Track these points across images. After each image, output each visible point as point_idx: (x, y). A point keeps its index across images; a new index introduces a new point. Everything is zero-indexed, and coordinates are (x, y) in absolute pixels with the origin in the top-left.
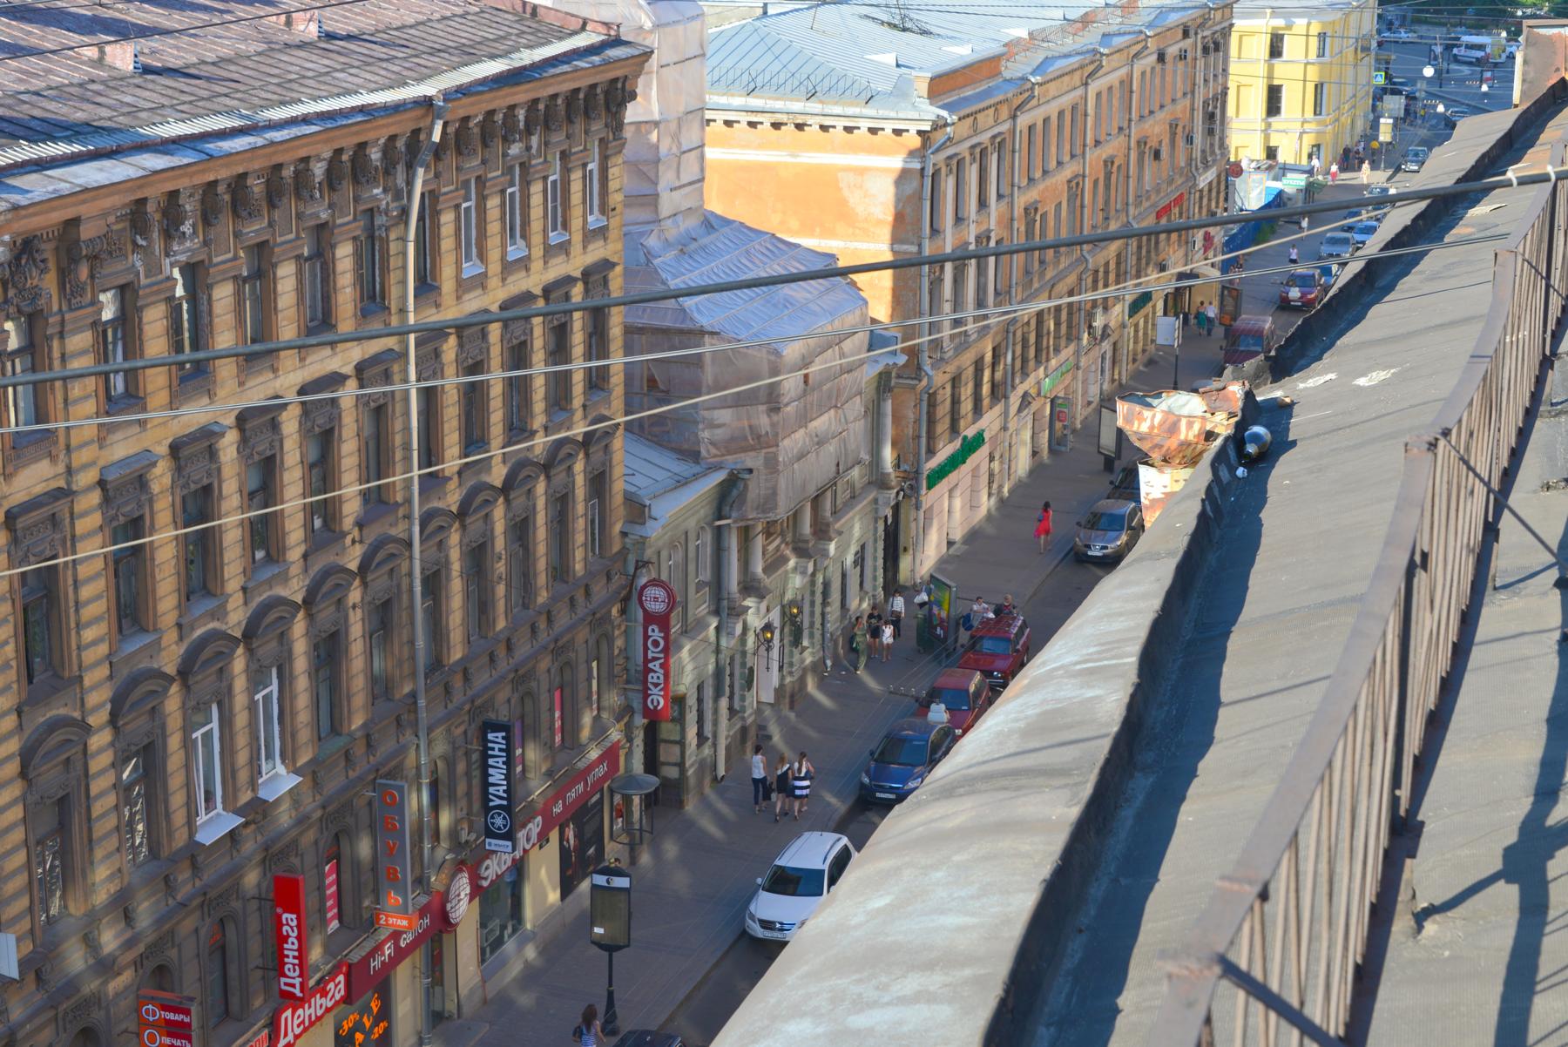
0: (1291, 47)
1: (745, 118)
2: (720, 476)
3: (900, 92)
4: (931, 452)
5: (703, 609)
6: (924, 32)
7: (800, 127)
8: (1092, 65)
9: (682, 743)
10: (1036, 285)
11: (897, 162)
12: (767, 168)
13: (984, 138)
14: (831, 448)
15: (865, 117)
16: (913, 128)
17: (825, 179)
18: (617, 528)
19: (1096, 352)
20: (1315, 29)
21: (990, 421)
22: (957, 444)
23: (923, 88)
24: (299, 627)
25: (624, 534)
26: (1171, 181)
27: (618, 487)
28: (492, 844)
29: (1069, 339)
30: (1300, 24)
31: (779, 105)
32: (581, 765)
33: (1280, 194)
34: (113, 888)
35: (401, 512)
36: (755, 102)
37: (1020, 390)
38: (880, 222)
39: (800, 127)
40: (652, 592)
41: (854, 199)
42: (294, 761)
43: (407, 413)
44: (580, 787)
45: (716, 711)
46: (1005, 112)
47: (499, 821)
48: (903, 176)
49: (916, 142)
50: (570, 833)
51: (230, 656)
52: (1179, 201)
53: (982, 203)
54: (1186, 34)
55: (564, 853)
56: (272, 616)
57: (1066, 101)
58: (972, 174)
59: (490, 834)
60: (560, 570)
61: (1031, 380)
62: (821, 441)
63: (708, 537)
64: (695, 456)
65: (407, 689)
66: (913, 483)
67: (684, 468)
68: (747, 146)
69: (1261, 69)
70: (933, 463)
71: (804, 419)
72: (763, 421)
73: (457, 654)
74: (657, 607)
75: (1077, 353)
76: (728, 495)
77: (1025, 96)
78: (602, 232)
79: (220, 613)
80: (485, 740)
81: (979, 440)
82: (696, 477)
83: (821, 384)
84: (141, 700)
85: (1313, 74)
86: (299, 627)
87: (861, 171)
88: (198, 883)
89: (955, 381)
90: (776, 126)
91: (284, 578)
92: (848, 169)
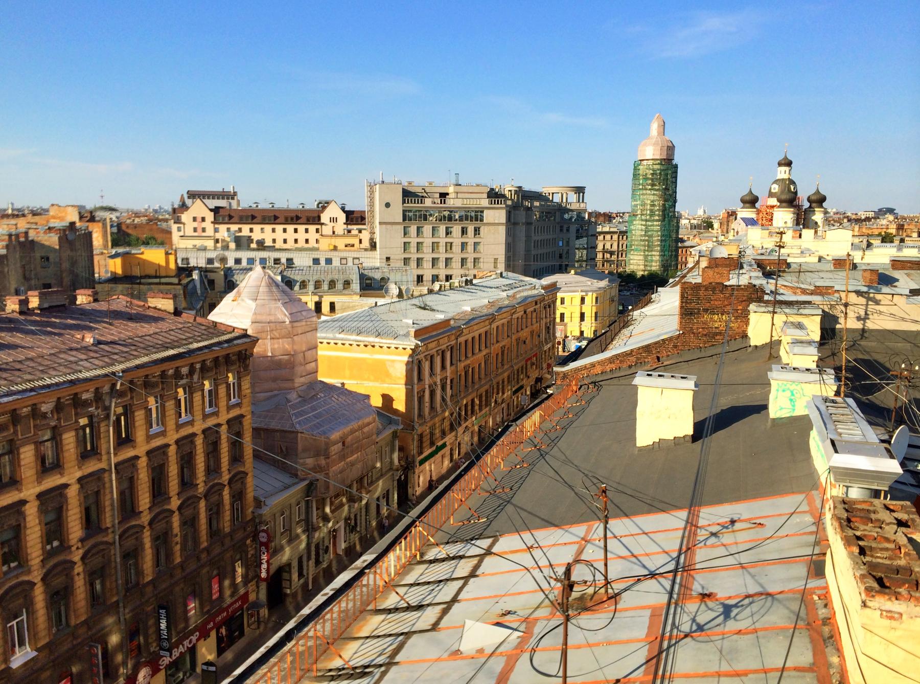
0: (588, 300)
1: (355, 343)
2: (306, 482)
3: (407, 335)
4: (421, 453)
5: (299, 531)
6: (433, 310)
7: (373, 346)
8: (492, 318)
9: (290, 580)
10: (470, 390)
11: (405, 358)
12: (364, 360)
13: (443, 347)
14: (359, 466)
15: (394, 343)
16: (408, 348)
17: (382, 363)
18: (250, 510)
19: (500, 408)
20: (595, 295)
21: (449, 439)
22: (434, 448)
23: (412, 334)
24: (202, 504)
25: (253, 512)
26: (532, 349)
27: (250, 495)
28: (162, 653)
29: (486, 406)
30: (590, 294)
31: (366, 339)
32: (225, 606)
33: (580, 347)
34: (47, 640)
35: (110, 531)
36: (359, 338)
37: (464, 425)
38: (400, 378)
39: (373, 346)
40: (263, 534)
41: (391, 370)
42: (36, 643)
43: (112, 492)
44: (225, 614)
45: (308, 566)
46: (453, 337)
47: (165, 644)
48: (408, 364)
49: (411, 352)
50: (223, 631)
51: (223, 489)
52: (536, 355)
53: (443, 367)
54: (536, 304)
55: (219, 640)
56: (239, 477)
57: (483, 331)
58: (438, 360)
59: (162, 649)
60: (214, 533)
61: (470, 421)
62: (352, 464)
63: (303, 504)
64: (296, 476)
65: (115, 599)
66: (408, 467)
67: (287, 480)
68: (356, 352)
69: (579, 308)
70: (422, 457)
71: (343, 457)
72: (323, 462)
73: (178, 560)
74: (264, 540)
75: (490, 410)
76: (310, 488)
77: (459, 331)
78: (238, 405)
79: (221, 476)
80: (159, 613)
81: (444, 445)
82: (294, 484)
83: (352, 445)
84: (132, 535)
85: (594, 310)
86: (202, 504)
87: (393, 361)
88: (90, 633)
89: (498, 383)
90: (366, 346)
91: (29, 572)
92: (388, 360)
